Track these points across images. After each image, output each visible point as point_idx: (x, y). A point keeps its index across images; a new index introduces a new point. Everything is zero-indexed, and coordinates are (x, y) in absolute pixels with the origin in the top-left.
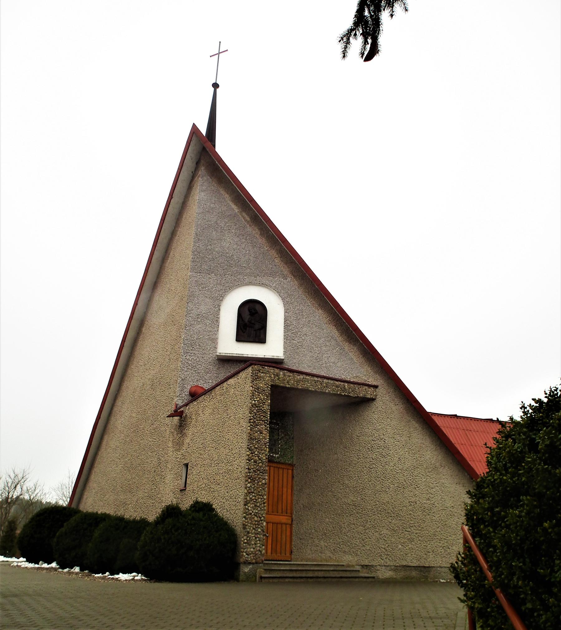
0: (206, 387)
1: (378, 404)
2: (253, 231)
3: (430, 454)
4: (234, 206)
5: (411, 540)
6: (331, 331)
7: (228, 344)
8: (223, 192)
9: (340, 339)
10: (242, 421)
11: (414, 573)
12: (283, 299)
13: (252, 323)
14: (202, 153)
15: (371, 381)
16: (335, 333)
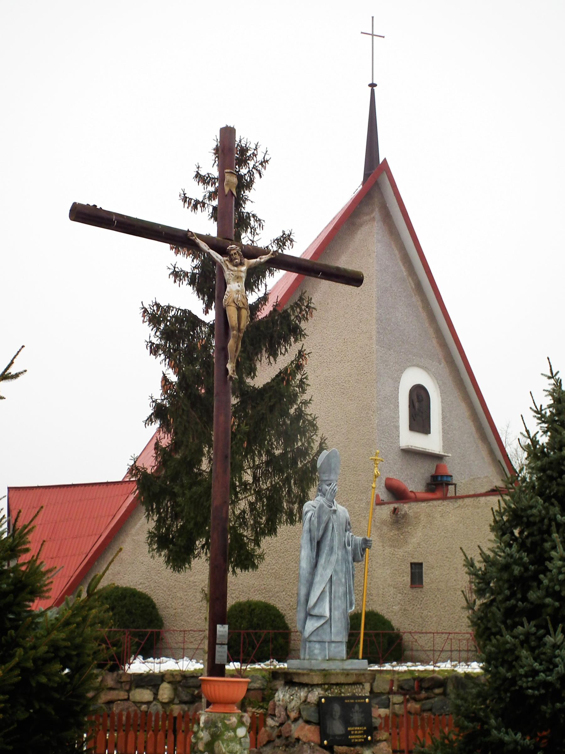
2: (416, 300)
6: (470, 427)
8: (393, 246)
12: (440, 387)
16: (473, 430)
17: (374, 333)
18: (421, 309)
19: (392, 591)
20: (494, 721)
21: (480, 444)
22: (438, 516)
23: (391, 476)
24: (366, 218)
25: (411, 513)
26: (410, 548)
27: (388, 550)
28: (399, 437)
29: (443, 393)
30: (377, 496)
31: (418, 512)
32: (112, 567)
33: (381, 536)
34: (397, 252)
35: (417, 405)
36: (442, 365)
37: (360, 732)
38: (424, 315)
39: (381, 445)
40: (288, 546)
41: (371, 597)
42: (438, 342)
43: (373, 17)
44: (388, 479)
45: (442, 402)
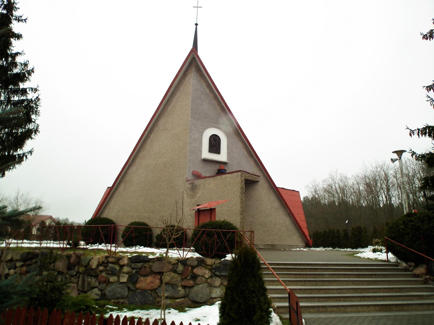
0: (203, 175)
1: (260, 183)
2: (214, 102)
3: (276, 204)
4: (207, 89)
5: (269, 235)
6: (244, 152)
7: (206, 154)
8: (202, 82)
9: (247, 155)
10: (236, 192)
11: (270, 247)
12: (227, 136)
13: (215, 144)
14: (193, 64)
15: (258, 174)
16: (246, 153)
17: (190, 114)
18: (217, 106)
19: (190, 217)
21: (249, 159)
23: (196, 170)
25: (198, 184)
26: (196, 198)
27: (189, 200)
30: (187, 178)
32: (184, 210)
33: (187, 194)
34: (204, 84)
35: (213, 142)
38: (218, 108)
44: (193, 171)
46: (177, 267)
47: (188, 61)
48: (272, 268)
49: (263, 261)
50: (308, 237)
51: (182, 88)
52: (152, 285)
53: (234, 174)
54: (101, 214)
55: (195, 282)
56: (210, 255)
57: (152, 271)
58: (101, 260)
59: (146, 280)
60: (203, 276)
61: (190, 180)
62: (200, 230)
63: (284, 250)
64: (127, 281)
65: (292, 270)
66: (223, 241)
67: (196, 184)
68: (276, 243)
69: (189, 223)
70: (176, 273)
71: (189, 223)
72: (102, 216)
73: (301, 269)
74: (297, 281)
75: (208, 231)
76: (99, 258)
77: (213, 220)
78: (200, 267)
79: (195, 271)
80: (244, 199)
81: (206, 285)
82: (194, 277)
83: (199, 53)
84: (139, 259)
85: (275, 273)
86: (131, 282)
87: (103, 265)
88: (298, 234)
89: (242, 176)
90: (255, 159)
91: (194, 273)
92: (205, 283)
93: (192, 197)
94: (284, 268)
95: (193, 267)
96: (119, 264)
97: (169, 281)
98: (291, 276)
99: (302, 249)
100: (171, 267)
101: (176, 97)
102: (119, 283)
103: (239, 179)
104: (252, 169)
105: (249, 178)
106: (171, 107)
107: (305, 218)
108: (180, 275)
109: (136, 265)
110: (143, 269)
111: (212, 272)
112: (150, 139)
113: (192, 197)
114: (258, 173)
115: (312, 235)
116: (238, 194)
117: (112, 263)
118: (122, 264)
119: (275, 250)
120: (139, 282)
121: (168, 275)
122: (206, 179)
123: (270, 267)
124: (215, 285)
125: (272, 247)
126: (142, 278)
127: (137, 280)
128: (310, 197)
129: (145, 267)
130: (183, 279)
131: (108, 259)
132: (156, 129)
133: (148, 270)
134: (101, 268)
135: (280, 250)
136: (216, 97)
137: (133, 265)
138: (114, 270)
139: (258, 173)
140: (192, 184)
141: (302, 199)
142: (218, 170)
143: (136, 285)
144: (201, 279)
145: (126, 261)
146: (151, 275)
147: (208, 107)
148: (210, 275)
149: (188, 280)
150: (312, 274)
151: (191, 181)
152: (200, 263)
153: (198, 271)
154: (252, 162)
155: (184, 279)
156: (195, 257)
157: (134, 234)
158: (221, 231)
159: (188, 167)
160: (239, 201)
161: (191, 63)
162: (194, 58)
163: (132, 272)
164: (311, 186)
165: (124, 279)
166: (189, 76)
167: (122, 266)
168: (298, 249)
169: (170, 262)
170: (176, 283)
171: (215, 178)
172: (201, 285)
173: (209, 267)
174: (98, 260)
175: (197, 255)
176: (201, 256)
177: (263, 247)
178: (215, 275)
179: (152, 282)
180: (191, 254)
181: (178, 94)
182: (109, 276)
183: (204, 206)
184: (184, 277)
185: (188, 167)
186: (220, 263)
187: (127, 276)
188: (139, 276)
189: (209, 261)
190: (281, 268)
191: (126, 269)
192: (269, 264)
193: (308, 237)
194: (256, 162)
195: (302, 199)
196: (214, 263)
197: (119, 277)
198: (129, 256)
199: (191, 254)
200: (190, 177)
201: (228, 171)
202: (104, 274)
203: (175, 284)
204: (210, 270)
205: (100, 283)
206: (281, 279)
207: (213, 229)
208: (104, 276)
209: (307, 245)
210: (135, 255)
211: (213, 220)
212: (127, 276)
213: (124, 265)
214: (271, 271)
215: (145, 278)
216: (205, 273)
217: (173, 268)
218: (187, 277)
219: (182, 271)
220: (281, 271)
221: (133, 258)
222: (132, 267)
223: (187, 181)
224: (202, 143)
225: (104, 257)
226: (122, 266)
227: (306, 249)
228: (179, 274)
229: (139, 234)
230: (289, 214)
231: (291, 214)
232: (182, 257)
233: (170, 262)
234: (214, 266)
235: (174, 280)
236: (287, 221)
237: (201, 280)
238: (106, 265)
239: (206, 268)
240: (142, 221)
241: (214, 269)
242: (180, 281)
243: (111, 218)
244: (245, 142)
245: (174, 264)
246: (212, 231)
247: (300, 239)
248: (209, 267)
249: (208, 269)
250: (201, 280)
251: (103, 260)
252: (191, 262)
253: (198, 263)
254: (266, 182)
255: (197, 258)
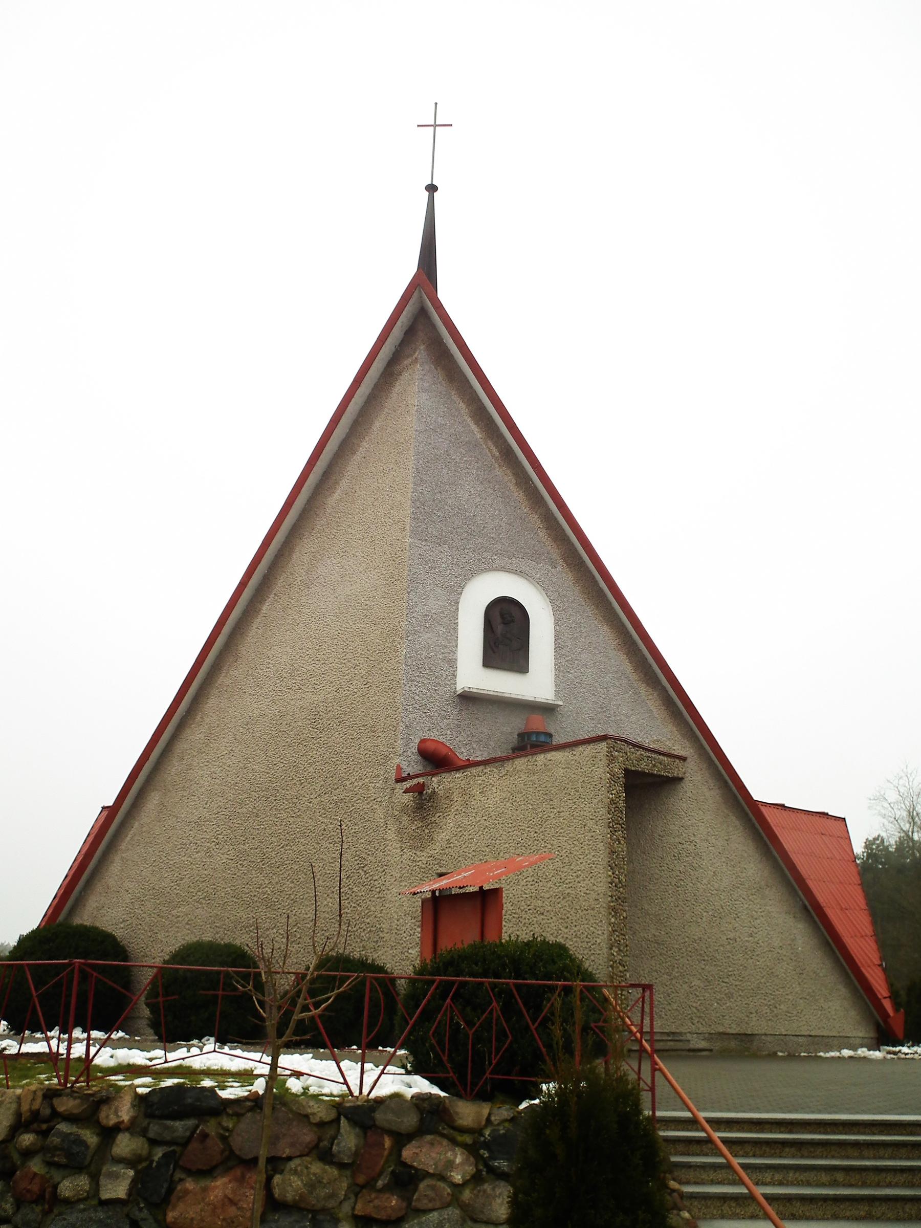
0: (463, 754)
2: (503, 474)
3: (753, 868)
4: (473, 427)
5: (729, 996)
6: (620, 662)
7: (472, 673)
8: (455, 398)
9: (634, 677)
10: (590, 824)
11: (733, 1044)
12: (552, 601)
13: (506, 633)
14: (420, 332)
15: (678, 750)
16: (628, 667)
17: (408, 520)
18: (512, 487)
20: (160, 1155)
21: (643, 689)
22: (476, 791)
23: (433, 735)
24: (407, 362)
26: (435, 849)
27: (408, 853)
28: (455, 676)
29: (557, 610)
31: (450, 789)
33: (399, 832)
34: (462, 405)
35: (499, 628)
36: (559, 568)
37: (691, 1175)
38: (518, 495)
39: (413, 689)
40: (285, 857)
41: (381, 935)
42: (549, 535)
43: (436, 104)
44: (423, 741)
45: (556, 624)
46: (334, 1138)
47: (399, 323)
48: (725, 1141)
49: (690, 1110)
50: (887, 1005)
51: (377, 424)
52: (232, 1211)
53: (581, 748)
54: (71, 912)
55: (409, 1200)
56: (472, 1090)
57: (232, 1152)
58: (25, 1107)
59: (205, 1190)
60: (442, 1178)
61: (410, 777)
62: (433, 981)
63: (792, 1057)
64: (129, 1194)
65: (819, 1150)
66: (527, 1027)
67: (434, 792)
68: (756, 1026)
69: (400, 949)
70: (331, 1163)
71: (400, 949)
72: (77, 921)
73: (856, 1144)
74: (837, 1199)
75: (463, 984)
76: (19, 1098)
77: (490, 938)
78: (429, 1137)
79: (407, 1153)
80: (622, 848)
81: (454, 1213)
82: (406, 1179)
83: (443, 295)
84: (184, 1105)
85: (736, 1162)
86: (145, 1200)
87: (35, 1126)
88: (843, 991)
89: (611, 759)
90: (664, 689)
91: (404, 1164)
92: (448, 1205)
93: (419, 841)
94: (784, 1143)
95: (402, 1139)
96: (98, 1122)
97: (301, 1195)
98: (811, 1176)
99: (862, 1052)
100: (308, 1136)
101: (358, 457)
102: (94, 1202)
103: (600, 771)
104: (652, 729)
105: (644, 766)
106: (336, 496)
107: (874, 923)
108: (348, 1173)
109: (167, 1127)
110: (194, 1145)
111: (478, 1158)
112: (258, 621)
113: (419, 841)
114: (680, 747)
115: (903, 993)
116: (600, 830)
117: (70, 1118)
118: (112, 1121)
119: (755, 1056)
120: (179, 1198)
121: (295, 1172)
122: (474, 770)
123: (716, 1135)
124: (493, 1216)
125: (742, 1047)
126: (190, 1184)
127: (171, 1190)
128: (893, 842)
129: (205, 1136)
130: (357, 1190)
131: (56, 1101)
132: (280, 583)
133: (215, 1147)
134: (27, 1139)
135: (773, 1056)
136: (507, 455)
137: (154, 1129)
138: (75, 1149)
139: (680, 747)
140: (419, 789)
141: (858, 848)
142: (521, 735)
143: (165, 1215)
144: (433, 1188)
145: (125, 1112)
146: (228, 1170)
147: (479, 492)
148: (470, 1169)
149: (380, 1191)
150: (903, 1170)
151: (415, 781)
152: (429, 1114)
153: (424, 1154)
154: (652, 702)
155: (363, 1187)
156: (409, 1093)
157: (220, 992)
158: (518, 987)
159: (402, 727)
160: (602, 857)
161: (410, 333)
162: (422, 312)
163: (149, 1158)
164: (892, 796)
165: (117, 1188)
166: (406, 376)
167: (109, 1133)
168: (846, 1053)
169: (305, 1117)
170: (331, 1204)
171: (509, 766)
172: (434, 1215)
173: (468, 1139)
174: (14, 1106)
175: (421, 1085)
176: (435, 1090)
177: (703, 1044)
178: (492, 1170)
179: (232, 1202)
180: (392, 1081)
181: (364, 448)
182: (56, 1175)
183: (463, 878)
184: (361, 1179)
185: (402, 727)
186: (512, 1120)
187: (131, 1173)
188: (178, 1175)
189: (468, 1112)
190: (768, 1142)
191: (124, 1145)
192: (709, 1121)
193: (887, 1005)
194: (668, 702)
195: (858, 848)
196: (488, 1120)
197: (95, 1178)
198: (140, 1091)
199: (392, 1081)
200: (411, 764)
201: (558, 739)
202: (36, 1166)
203: (324, 1210)
204: (472, 1150)
205: (19, 1204)
206: (759, 1191)
207: (485, 974)
208: (35, 1174)
209: (884, 1036)
210: (169, 1082)
211: (490, 938)
212: (131, 1173)
213: (117, 1129)
214: (722, 1155)
215: (203, 1183)
216: (450, 1164)
217: (320, 1140)
218: (375, 1180)
219: (356, 1153)
220: (772, 1156)
221: (155, 1099)
222: (151, 1135)
223: (400, 780)
224: (456, 630)
225: (40, 1094)
226: (109, 1133)
227: (877, 1055)
228: (341, 1166)
229: (211, 993)
230: (805, 908)
231: (814, 913)
232: (356, 1093)
233: (307, 1116)
234: (487, 1132)
235: (322, 1192)
236: (798, 936)
237: (430, 1193)
238: (44, 1126)
239: (454, 1142)
240: (227, 940)
241: (486, 1145)
242: (346, 1198)
243: (110, 929)
244: (623, 625)
245: (322, 1124)
246: (482, 983)
247: (853, 1013)
248: (468, 1139)
249: (464, 1146)
250: (430, 1193)
251: (37, 1105)
252: (390, 1116)
253: (422, 1120)
254: (711, 783)
255: (421, 1099)
